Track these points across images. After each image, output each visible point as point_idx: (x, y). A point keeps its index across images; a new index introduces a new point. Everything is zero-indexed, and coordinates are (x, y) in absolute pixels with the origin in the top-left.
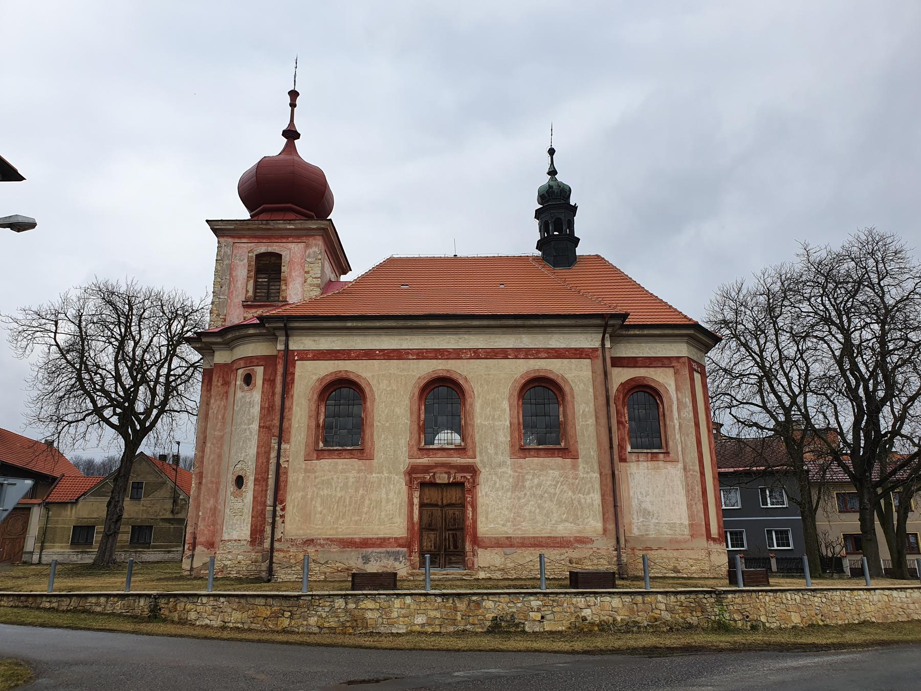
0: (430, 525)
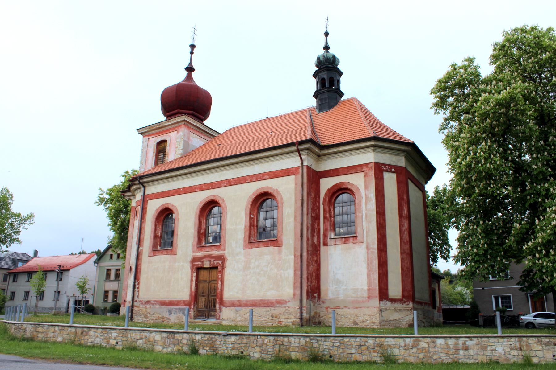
0: (203, 293)
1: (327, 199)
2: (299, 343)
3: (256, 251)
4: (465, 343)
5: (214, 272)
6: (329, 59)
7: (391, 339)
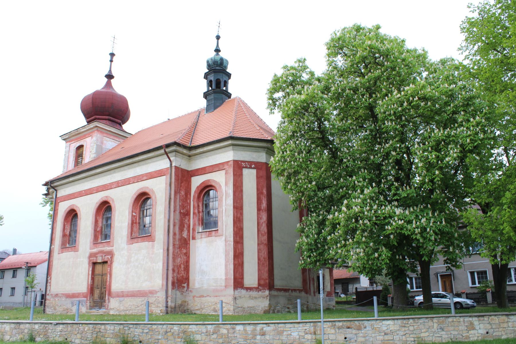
1: (196, 196)
2: (114, 330)
3: (136, 245)
4: (262, 329)
5: (106, 266)
6: (217, 62)
7: (194, 326)
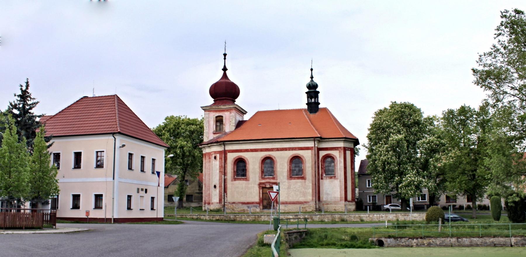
3: (293, 181)
